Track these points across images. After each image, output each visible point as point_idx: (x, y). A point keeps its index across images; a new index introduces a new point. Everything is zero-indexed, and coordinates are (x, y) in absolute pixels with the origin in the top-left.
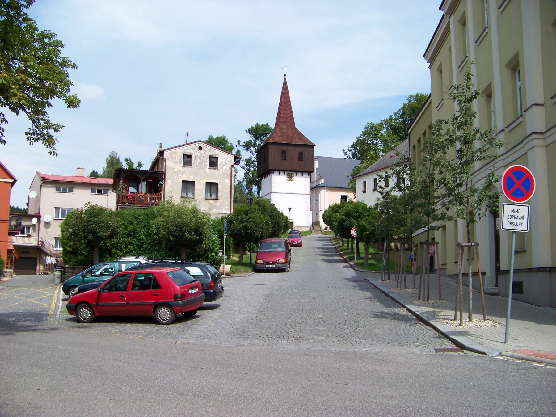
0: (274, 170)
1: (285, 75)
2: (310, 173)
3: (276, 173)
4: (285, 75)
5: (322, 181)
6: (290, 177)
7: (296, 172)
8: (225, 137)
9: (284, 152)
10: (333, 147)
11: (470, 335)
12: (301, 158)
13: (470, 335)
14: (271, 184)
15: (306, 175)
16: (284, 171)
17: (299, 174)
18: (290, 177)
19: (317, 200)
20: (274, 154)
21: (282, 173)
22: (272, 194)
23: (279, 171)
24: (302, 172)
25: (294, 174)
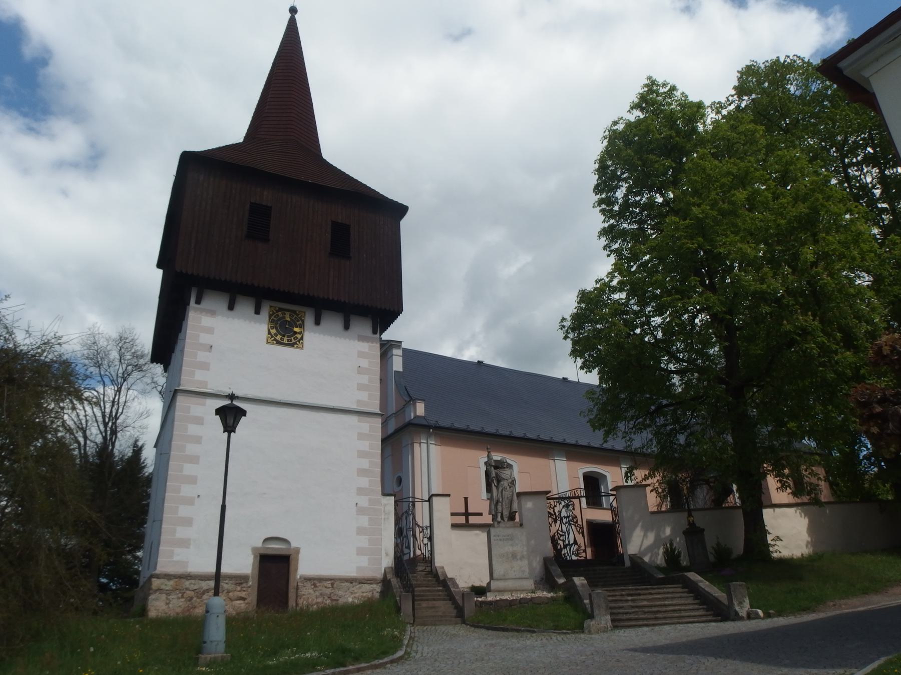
1: (293, 10)
4: (293, 10)
5: (420, 409)
6: (286, 332)
15: (362, 327)
17: (333, 322)
18: (286, 332)
21: (245, 307)
25: (309, 320)
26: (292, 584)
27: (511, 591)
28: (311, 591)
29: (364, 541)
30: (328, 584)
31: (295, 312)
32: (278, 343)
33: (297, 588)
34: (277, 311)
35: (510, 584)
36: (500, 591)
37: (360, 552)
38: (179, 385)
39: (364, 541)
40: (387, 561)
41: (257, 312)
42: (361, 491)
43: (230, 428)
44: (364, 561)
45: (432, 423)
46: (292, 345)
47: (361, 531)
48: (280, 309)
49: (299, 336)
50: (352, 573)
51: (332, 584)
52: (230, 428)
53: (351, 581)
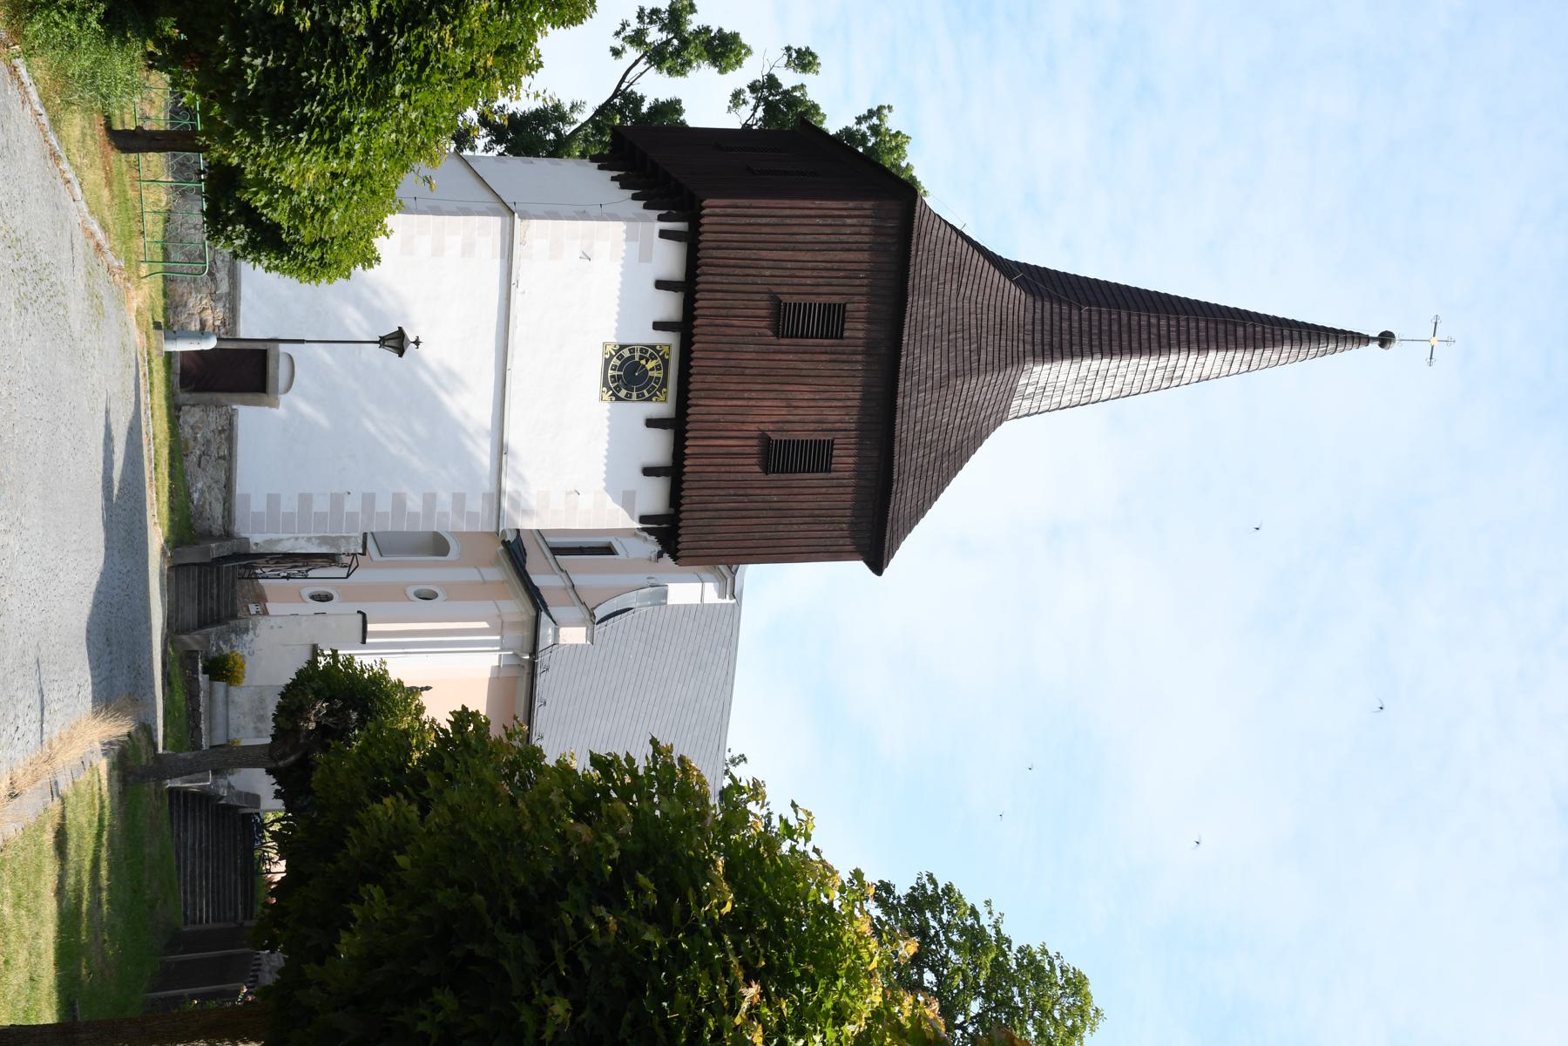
0: (691, 242)
1: (1385, 339)
2: (671, 535)
3: (668, 259)
4: (1385, 339)
5: (573, 635)
6: (627, 375)
7: (677, 425)
8: (722, 71)
9: (831, 321)
10: (832, 711)
11: (63, 817)
12: (781, 456)
13: (63, 817)
14: (583, 216)
15: (653, 498)
16: (684, 327)
17: (657, 447)
18: (627, 375)
19: (428, 596)
20: (818, 240)
21: (668, 306)
22: (495, 223)
23: (686, 286)
24: (673, 472)
25: (662, 408)
26: (223, 397)
27: (211, 718)
28: (213, 426)
29: (289, 505)
30: (224, 451)
31: (664, 385)
32: (607, 362)
33: (218, 405)
34: (662, 357)
35: (220, 708)
36: (211, 693)
37: (273, 500)
38: (522, 217)
39: (289, 505)
40: (258, 538)
41: (658, 326)
42: (369, 499)
43: (383, 341)
44: (258, 505)
45: (543, 659)
46: (605, 384)
47: (305, 499)
48: (666, 362)
49: (623, 393)
50: (241, 486)
51: (223, 458)
52: (383, 341)
53: (229, 486)
